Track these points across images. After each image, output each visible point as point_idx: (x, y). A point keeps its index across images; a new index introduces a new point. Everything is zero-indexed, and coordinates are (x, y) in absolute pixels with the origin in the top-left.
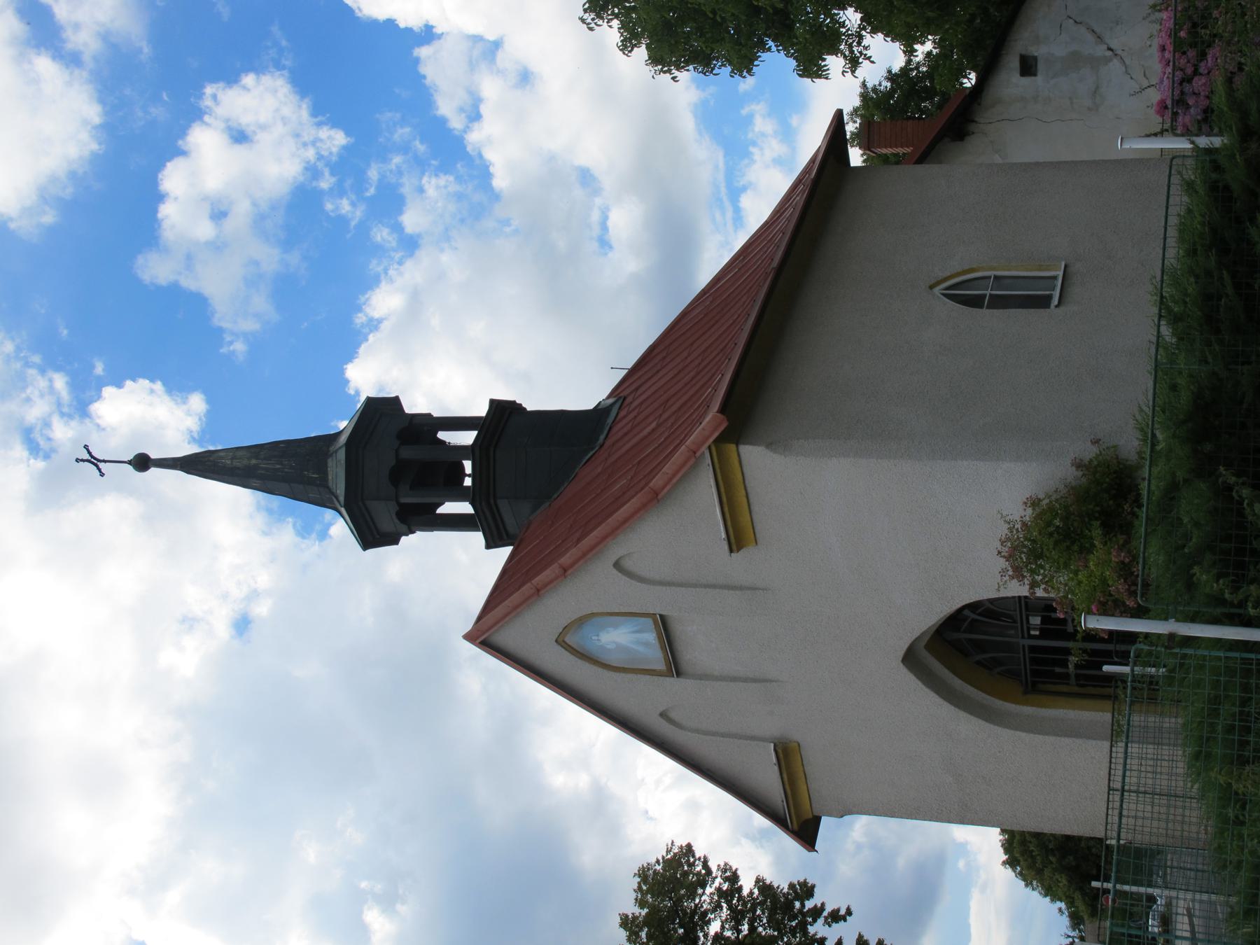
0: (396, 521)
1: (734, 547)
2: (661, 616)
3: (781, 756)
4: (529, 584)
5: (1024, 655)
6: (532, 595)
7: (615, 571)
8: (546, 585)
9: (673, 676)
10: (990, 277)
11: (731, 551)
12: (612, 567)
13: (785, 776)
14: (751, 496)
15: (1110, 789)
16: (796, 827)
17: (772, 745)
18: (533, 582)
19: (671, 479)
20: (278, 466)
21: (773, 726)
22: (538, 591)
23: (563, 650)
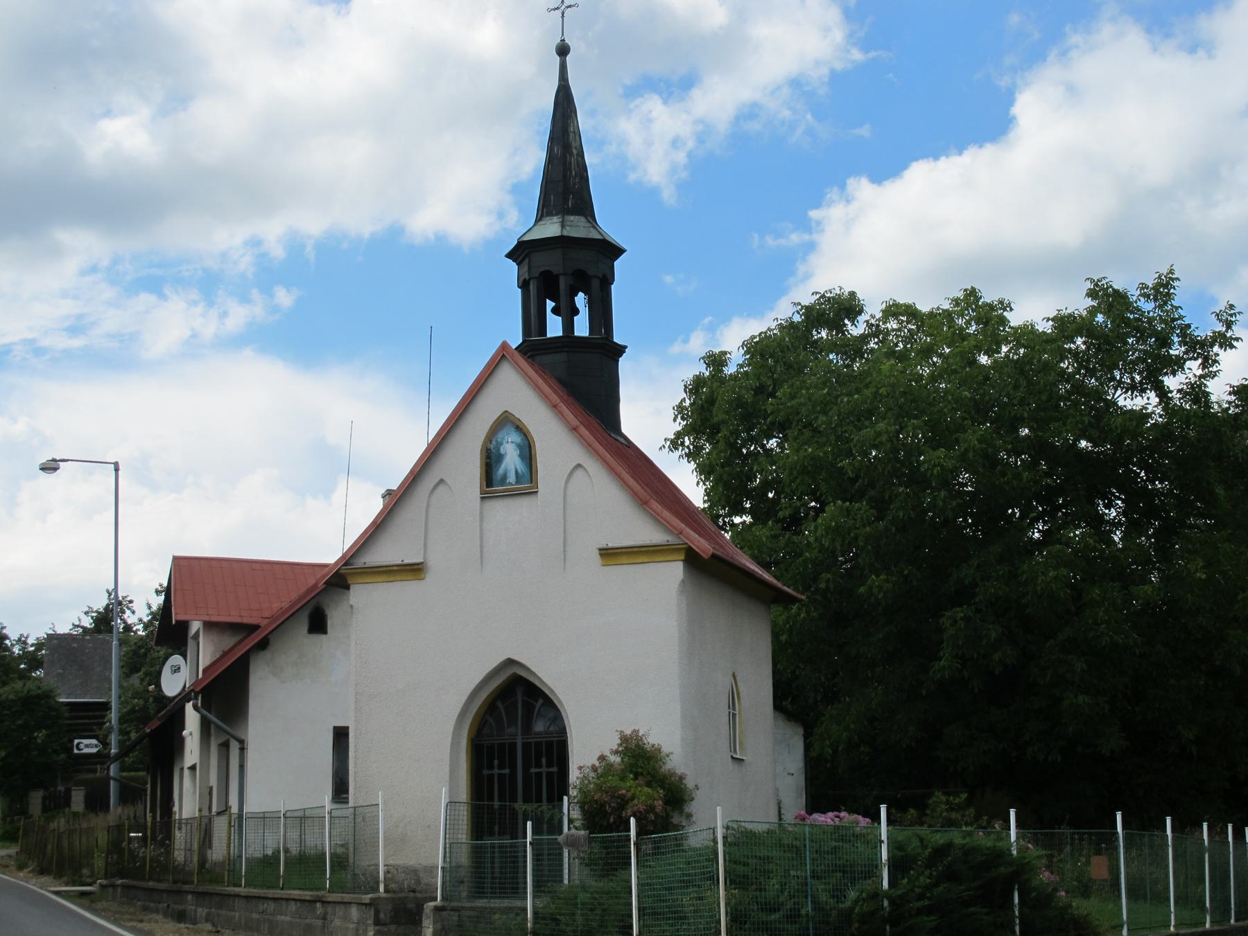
0: (546, 268)
1: (603, 552)
2: (537, 492)
3: (416, 567)
4: (559, 400)
5: (544, 737)
6: (551, 402)
7: (575, 464)
8: (560, 412)
9: (481, 494)
10: (735, 711)
11: (600, 550)
12: (577, 463)
13: (395, 568)
14: (642, 565)
15: (264, 812)
16: (342, 571)
17: (423, 561)
18: (561, 403)
19: (658, 515)
20: (574, 173)
21: (436, 562)
22: (555, 406)
23: (499, 415)
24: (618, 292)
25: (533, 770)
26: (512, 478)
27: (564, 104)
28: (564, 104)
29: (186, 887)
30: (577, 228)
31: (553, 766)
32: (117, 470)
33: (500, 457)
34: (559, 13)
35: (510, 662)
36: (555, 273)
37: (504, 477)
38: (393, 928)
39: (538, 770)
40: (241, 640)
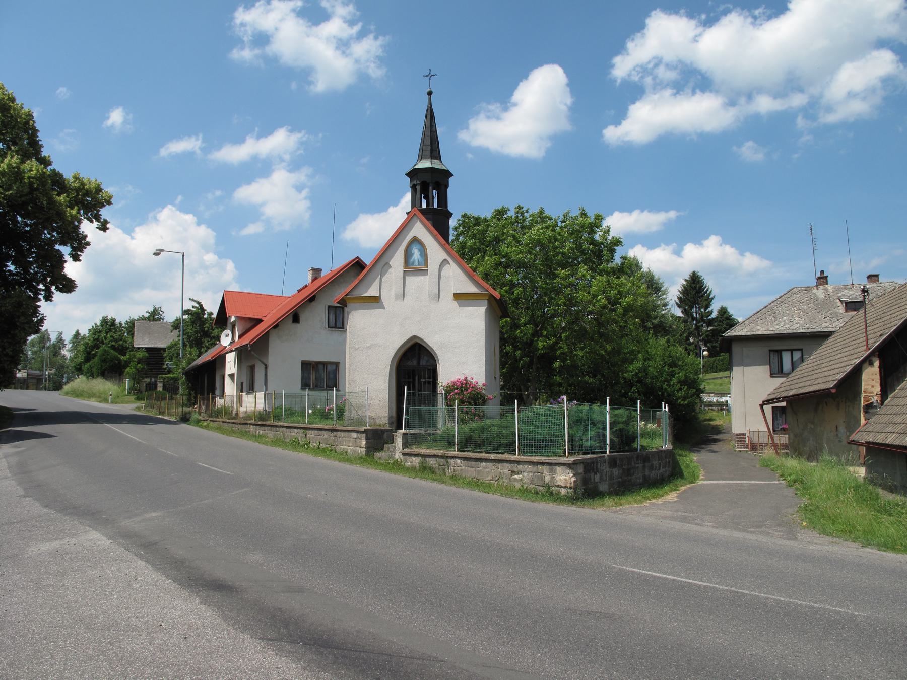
24: (450, 191)
25: (431, 380)
26: (416, 263)
27: (430, 115)
28: (430, 115)
29: (249, 422)
30: (437, 165)
31: (410, 379)
32: (183, 256)
33: (412, 255)
34: (428, 77)
35: (415, 337)
36: (428, 182)
37: (413, 263)
38: (372, 440)
39: (409, 380)
40: (250, 328)
